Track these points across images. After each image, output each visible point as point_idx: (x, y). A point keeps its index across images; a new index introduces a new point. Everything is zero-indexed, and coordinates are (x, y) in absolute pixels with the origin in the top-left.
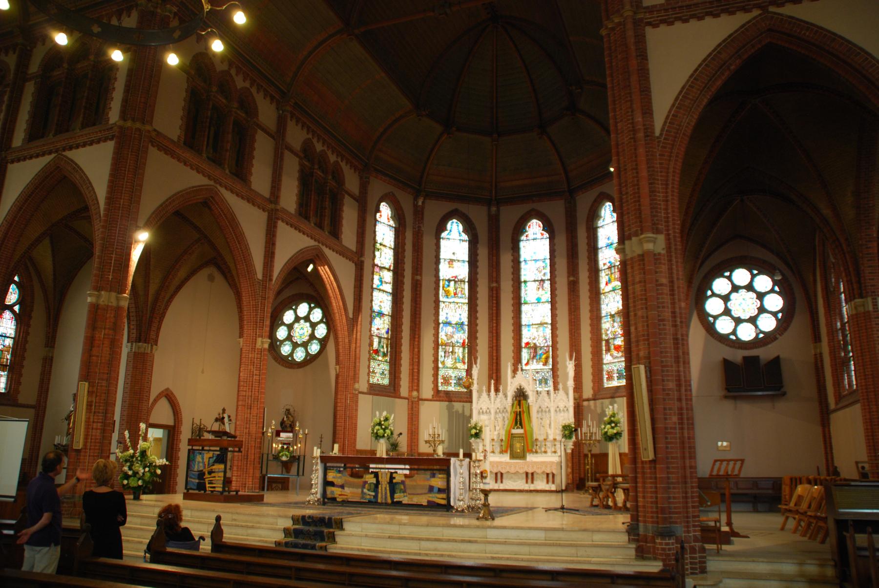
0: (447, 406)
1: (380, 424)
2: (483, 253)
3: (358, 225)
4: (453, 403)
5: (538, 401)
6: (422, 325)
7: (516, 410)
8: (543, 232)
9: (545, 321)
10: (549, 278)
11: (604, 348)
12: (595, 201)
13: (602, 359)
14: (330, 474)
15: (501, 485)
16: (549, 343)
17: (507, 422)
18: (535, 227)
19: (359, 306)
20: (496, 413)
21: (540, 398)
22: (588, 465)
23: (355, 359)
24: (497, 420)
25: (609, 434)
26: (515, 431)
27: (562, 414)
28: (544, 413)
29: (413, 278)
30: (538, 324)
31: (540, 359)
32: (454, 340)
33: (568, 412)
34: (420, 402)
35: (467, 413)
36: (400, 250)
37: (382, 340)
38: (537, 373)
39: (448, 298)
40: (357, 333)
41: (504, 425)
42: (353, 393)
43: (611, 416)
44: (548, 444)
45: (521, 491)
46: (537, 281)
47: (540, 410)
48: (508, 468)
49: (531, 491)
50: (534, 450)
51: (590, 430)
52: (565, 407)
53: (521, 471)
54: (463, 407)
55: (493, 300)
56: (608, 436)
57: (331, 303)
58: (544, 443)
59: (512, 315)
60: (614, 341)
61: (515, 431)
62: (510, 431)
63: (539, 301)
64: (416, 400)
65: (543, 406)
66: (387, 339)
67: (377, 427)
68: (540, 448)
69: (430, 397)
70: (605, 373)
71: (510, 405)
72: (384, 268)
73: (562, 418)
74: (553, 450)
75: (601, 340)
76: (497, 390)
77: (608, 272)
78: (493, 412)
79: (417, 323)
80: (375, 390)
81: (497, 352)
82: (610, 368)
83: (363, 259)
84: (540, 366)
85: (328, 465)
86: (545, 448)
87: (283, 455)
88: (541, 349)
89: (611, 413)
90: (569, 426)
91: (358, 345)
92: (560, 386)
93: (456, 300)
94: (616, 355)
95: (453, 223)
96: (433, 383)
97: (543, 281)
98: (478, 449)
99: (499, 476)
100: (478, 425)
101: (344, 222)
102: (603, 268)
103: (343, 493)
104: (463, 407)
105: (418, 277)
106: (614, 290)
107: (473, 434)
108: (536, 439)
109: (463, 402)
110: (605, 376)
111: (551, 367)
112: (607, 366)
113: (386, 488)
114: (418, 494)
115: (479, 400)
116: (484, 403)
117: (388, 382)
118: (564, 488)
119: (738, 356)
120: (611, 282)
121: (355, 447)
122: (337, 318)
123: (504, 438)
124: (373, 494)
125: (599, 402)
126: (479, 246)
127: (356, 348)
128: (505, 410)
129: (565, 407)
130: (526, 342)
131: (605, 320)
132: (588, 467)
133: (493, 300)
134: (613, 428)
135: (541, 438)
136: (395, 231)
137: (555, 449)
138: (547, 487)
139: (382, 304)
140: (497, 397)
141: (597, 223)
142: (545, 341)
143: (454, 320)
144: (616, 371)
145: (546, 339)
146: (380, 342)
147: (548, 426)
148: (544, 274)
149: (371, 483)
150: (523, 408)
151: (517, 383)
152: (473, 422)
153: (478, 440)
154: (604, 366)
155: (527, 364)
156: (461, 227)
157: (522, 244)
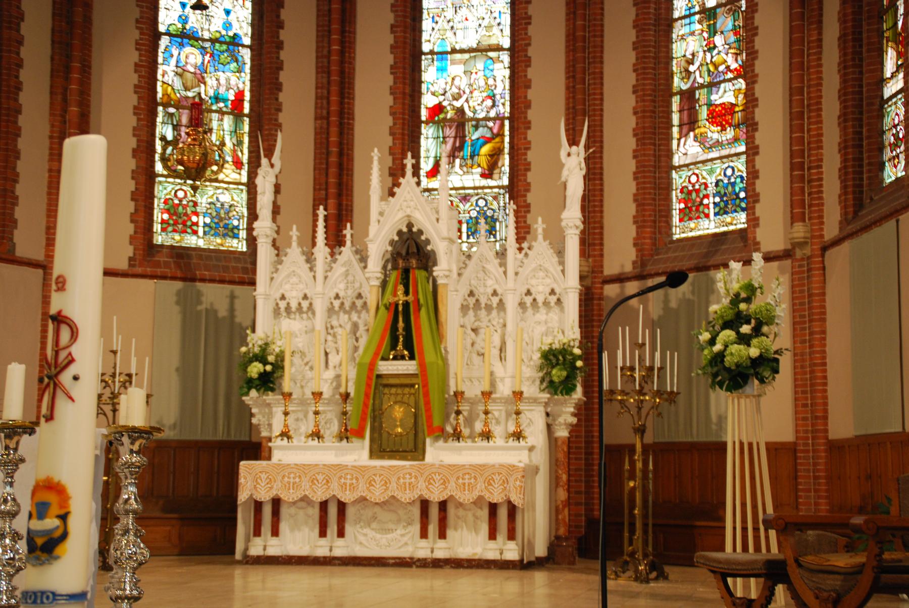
0: (178, 293)
4: (199, 285)
5: (467, 273)
6: (95, 31)
7: (392, 300)
9: (493, 41)
11: (675, 119)
13: (670, 154)
15: (340, 542)
16: (501, 109)
17: (363, 342)
20: (331, 311)
22: (632, 477)
24: (334, 336)
26: (388, 367)
27: (542, 315)
28: (483, 313)
30: (470, 50)
31: (472, 157)
32: (207, 91)
33: (562, 310)
35: (241, 318)
38: (465, 199)
41: (356, 349)
43: (736, 300)
44: (497, 410)
45: (403, 563)
47: (472, 301)
49: (437, 564)
50: (449, 429)
51: (642, 359)
52: (553, 292)
53: (406, 496)
54: (232, 297)
56: (728, 370)
58: (481, 408)
60: (710, 93)
61: (388, 367)
62: (372, 366)
65: (482, 290)
68: (470, 422)
70: (675, 195)
71: (377, 283)
73: (541, 329)
74: (512, 428)
76: (336, 241)
78: (320, 307)
81: (341, 134)
84: (474, 179)
86: (486, 424)
88: (476, 127)
89: (735, 286)
90: (564, 351)
92: (539, 226)
94: (716, 136)
98: (270, 425)
99: (333, 511)
100: (270, 350)
104: (232, 297)
108: (456, 394)
109: (232, 282)
110: (677, 206)
111: (505, 181)
112: (685, 173)
116: (294, 280)
118: (541, 550)
123: (352, 390)
128: (359, 303)
129: (553, 292)
130: (431, 105)
131: (685, 30)
132: (632, 484)
134: (745, 340)
135: (472, 391)
137: (518, 425)
138: (490, 551)
140: (335, 261)
142: (489, 103)
144: (711, 189)
145: (492, 97)
147: (496, 352)
150: (416, 293)
151: (400, 215)
152: (255, 340)
153: (270, 397)
154: (674, 175)
155: (434, 172)
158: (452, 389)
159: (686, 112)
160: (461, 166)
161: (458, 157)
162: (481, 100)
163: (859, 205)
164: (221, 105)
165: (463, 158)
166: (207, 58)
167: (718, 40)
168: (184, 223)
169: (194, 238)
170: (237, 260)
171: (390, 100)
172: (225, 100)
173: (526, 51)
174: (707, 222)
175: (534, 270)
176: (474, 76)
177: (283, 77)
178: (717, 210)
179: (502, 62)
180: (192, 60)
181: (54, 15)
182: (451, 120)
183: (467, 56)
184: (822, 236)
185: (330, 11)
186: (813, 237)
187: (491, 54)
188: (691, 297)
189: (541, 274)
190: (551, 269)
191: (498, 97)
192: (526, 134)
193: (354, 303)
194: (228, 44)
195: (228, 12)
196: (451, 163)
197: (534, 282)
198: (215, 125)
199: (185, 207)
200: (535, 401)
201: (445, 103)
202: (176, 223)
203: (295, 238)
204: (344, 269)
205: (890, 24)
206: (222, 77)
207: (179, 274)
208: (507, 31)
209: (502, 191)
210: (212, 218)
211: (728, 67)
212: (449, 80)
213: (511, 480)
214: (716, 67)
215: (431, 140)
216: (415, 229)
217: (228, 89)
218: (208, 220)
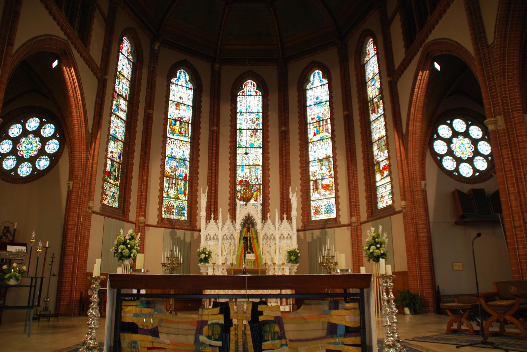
0: (170, 233)
1: (125, 243)
2: (206, 101)
3: (104, 44)
4: (176, 230)
8: (257, 90)
9: (257, 163)
10: (261, 128)
11: (312, 187)
12: (307, 68)
13: (310, 197)
14: (129, 308)
18: (250, 86)
19: (99, 123)
20: (223, 238)
21: (266, 226)
23: (91, 176)
25: (375, 254)
27: (285, 241)
28: (268, 240)
29: (145, 112)
32: (177, 173)
34: (146, 227)
36: (136, 83)
37: (115, 163)
39: (173, 135)
40: (94, 149)
42: (86, 212)
43: (374, 238)
46: (251, 129)
52: (289, 234)
54: (185, 234)
55: (213, 142)
57: (71, 113)
59: (229, 156)
64: (143, 225)
65: (268, 234)
66: (119, 163)
67: (122, 246)
69: (155, 224)
70: (312, 208)
72: (121, 96)
73: (285, 245)
75: (309, 180)
77: (316, 125)
78: (220, 238)
79: (148, 152)
80: (106, 211)
82: (318, 204)
83: (106, 77)
85: (124, 291)
87: (11, 277)
91: (95, 161)
93: (181, 138)
95: (181, 72)
96: (158, 211)
101: (93, 33)
102: (311, 122)
103: (156, 345)
104: (185, 234)
105: (151, 111)
106: (322, 139)
107: (203, 258)
108: (265, 264)
109: (185, 230)
110: (313, 211)
112: (315, 202)
113: (244, 333)
114: (308, 340)
115: (207, 227)
116: (212, 229)
117: (117, 205)
119: (466, 188)
120: (319, 133)
121: (85, 270)
122: (77, 130)
124: (219, 343)
125: (308, 233)
126: (203, 94)
127: (92, 165)
129: (289, 234)
130: (239, 180)
133: (213, 142)
136: (133, 66)
139: (117, 129)
141: (306, 87)
142: (256, 180)
143: (178, 156)
144: (323, 207)
145: (257, 179)
146: (112, 166)
148: (257, 124)
149: (213, 324)
151: (246, 212)
154: (312, 202)
156: (187, 77)
157: (239, 99)
158: (264, 262)
163: (372, 213)
164: (181, 177)
166: (178, 164)
167: (323, 167)
168: (170, 212)
169: (173, 216)
170: (185, 223)
171: (229, 178)
172: (182, 176)
175: (284, 228)
177: (199, 170)
180: (174, 164)
181: (141, 151)
184: (360, 221)
185: (212, 152)
186: (358, 221)
187: (257, 167)
188: (320, 236)
189: (285, 229)
190: (288, 228)
193: (230, 237)
194: (183, 160)
195: (184, 151)
197: (283, 231)
198: (179, 183)
199: (171, 207)
200: (287, 265)
202: (168, 211)
203: (229, 217)
204: (227, 227)
205: (378, 168)
206: (182, 169)
207: (171, 227)
208: (261, 161)
210: (178, 210)
214: (323, 174)
217: (183, 173)
218: (177, 211)
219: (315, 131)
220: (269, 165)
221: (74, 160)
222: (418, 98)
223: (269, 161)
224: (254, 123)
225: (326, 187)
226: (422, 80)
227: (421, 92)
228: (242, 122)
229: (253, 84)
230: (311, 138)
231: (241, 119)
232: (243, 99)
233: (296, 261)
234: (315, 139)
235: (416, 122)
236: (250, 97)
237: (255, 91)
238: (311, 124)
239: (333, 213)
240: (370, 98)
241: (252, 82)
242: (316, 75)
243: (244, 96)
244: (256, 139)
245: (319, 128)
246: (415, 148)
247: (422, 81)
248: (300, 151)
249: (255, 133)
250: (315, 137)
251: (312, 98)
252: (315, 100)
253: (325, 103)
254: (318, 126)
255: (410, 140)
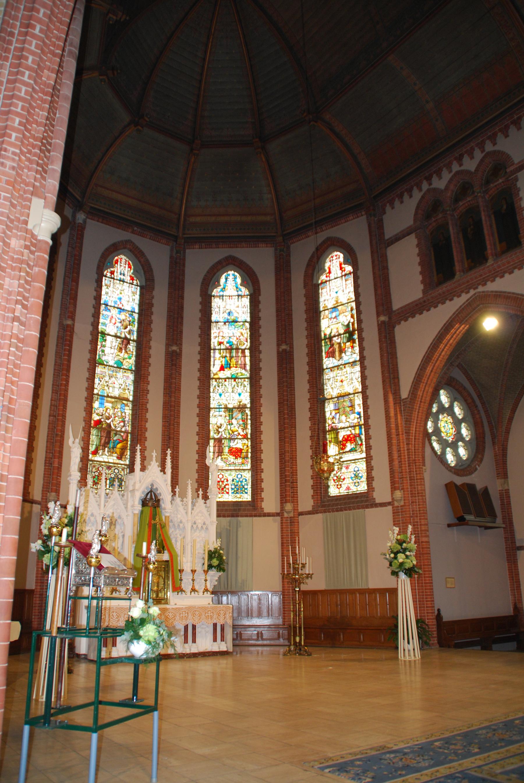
8: (133, 276)
9: (125, 396)
10: (135, 338)
30: (115, 398)
31: (113, 448)
46: (120, 337)
48: (215, 616)
63: (119, 366)
84: (113, 459)
88: (116, 434)
97: (126, 341)
111: (127, 462)
120: (230, 368)
128: (204, 527)
138: (215, 647)
142: (122, 424)
144: (230, 482)
145: (124, 421)
155: (95, 453)
159: (217, 448)
160: (108, 452)
161: (106, 447)
162: (118, 422)
165: (109, 448)
167: (234, 421)
173: (146, 405)
174: (227, 495)
176: (116, 410)
178: (233, 491)
179: (129, 406)
182: (105, 429)
183: (113, 400)
187: (125, 402)
189: (200, 514)
191: (126, 422)
192: (145, 443)
196: (104, 450)
201: (102, 420)
208: (132, 393)
209: (126, 467)
211: (239, 434)
212: (105, 409)
213: (227, 613)
215: (94, 436)
216: (155, 487)
219: (223, 363)
220: (147, 403)
221: (420, 381)
222: (441, 356)
223: (149, 396)
224: (126, 328)
225: (236, 453)
226: (456, 335)
227: (448, 349)
228: (107, 322)
229: (129, 264)
230: (215, 372)
231: (106, 317)
232: (112, 283)
233: (220, 568)
234: (222, 374)
235: (429, 387)
236: (122, 283)
237: (131, 276)
238: (217, 351)
239: (246, 493)
240: (325, 335)
241: (127, 259)
242: (231, 278)
243: (114, 279)
244: (126, 356)
245: (230, 360)
246: (421, 421)
247: (454, 336)
248: (199, 389)
249: (126, 345)
250: (222, 372)
251: (221, 312)
252: (226, 315)
253: (242, 323)
254: (228, 355)
255: (416, 409)
